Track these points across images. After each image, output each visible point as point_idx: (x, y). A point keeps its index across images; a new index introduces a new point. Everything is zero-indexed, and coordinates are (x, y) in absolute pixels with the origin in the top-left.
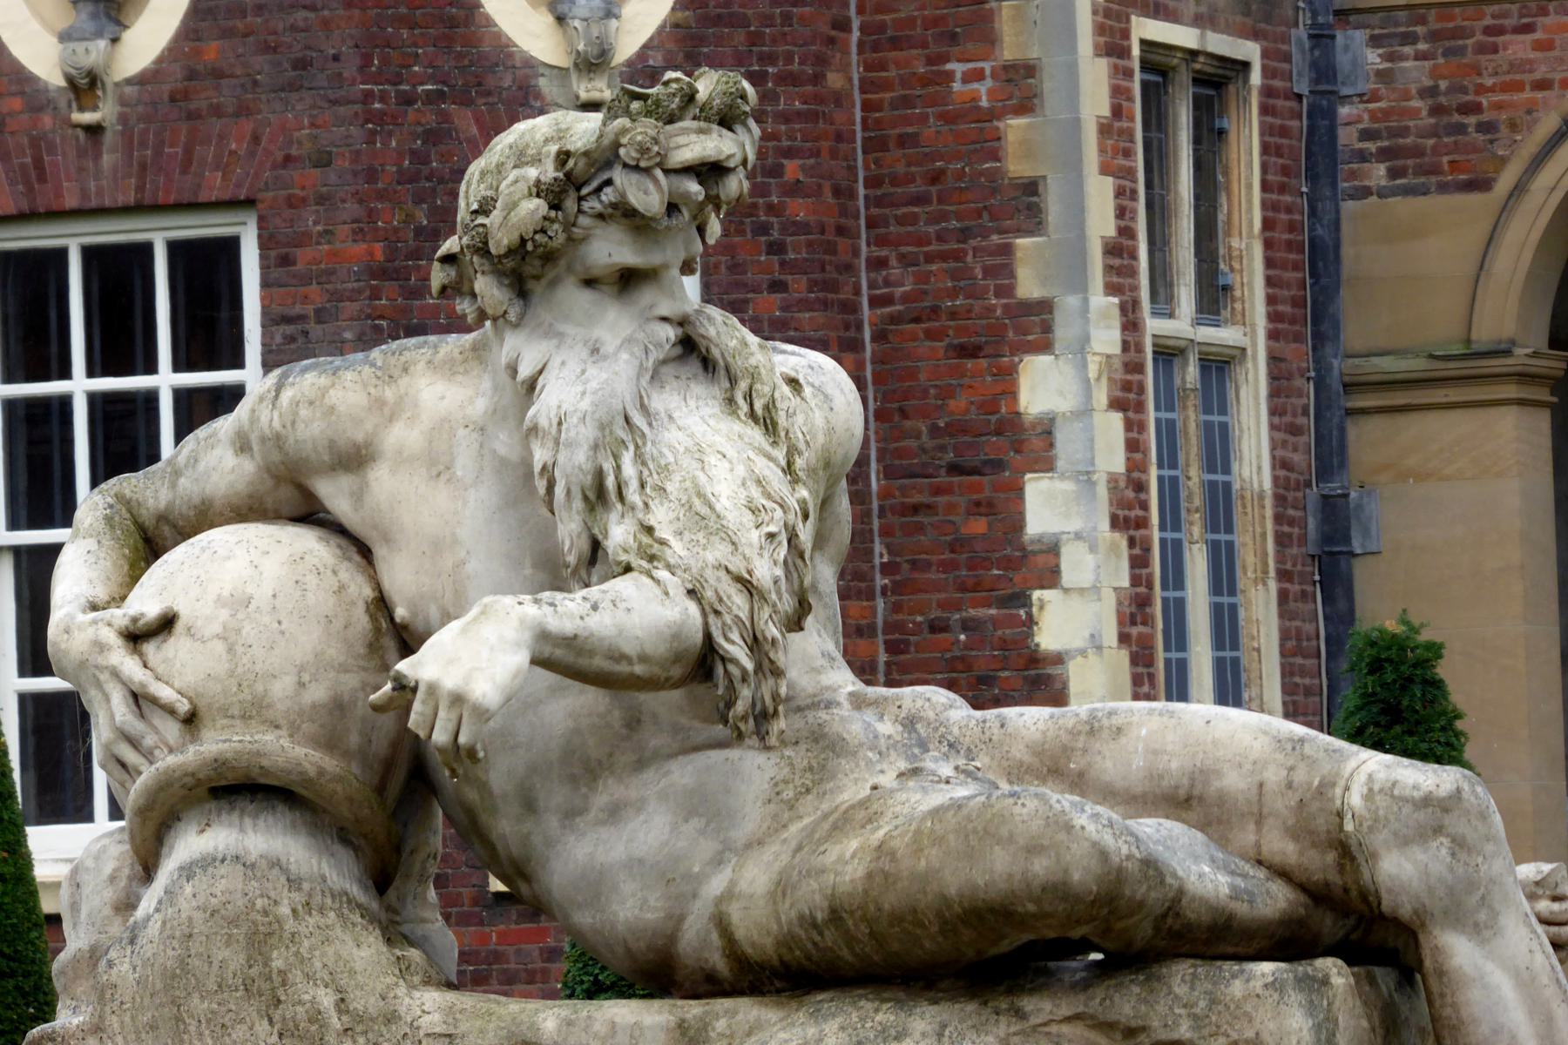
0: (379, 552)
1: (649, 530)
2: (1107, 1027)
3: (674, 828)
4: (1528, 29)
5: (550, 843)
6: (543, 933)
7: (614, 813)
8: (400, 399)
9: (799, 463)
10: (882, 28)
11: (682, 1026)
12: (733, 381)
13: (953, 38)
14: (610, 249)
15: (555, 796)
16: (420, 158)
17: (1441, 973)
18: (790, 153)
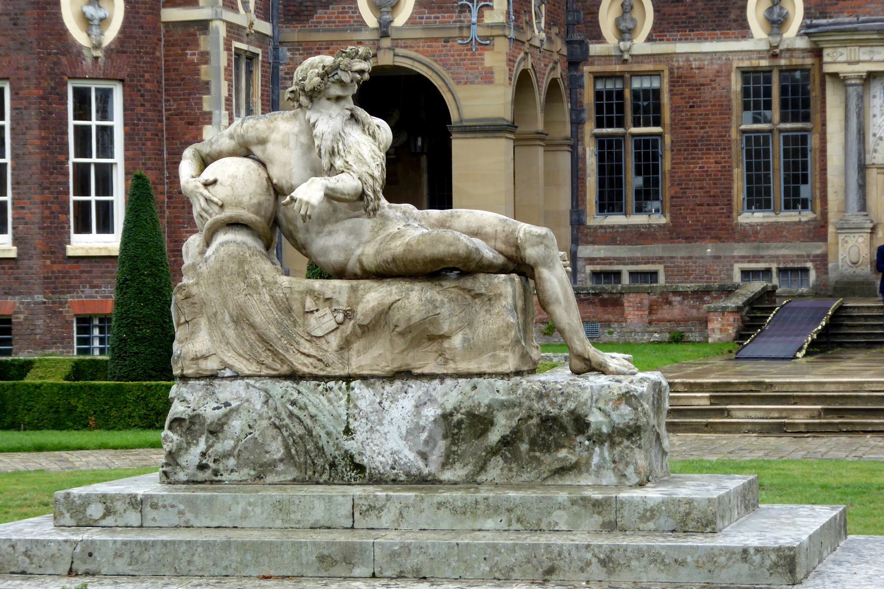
0: (269, 166)
1: (347, 162)
2: (463, 289)
3: (347, 237)
4: (328, 48)
5: (313, 240)
6: (80, 266)
7: (330, 233)
8: (275, 127)
9: (381, 147)
10: (169, 41)
11: (352, 286)
12: (364, 126)
13: (188, 44)
14: (335, 91)
15: (314, 228)
16: (52, 69)
17: (540, 278)
18: (146, 72)
